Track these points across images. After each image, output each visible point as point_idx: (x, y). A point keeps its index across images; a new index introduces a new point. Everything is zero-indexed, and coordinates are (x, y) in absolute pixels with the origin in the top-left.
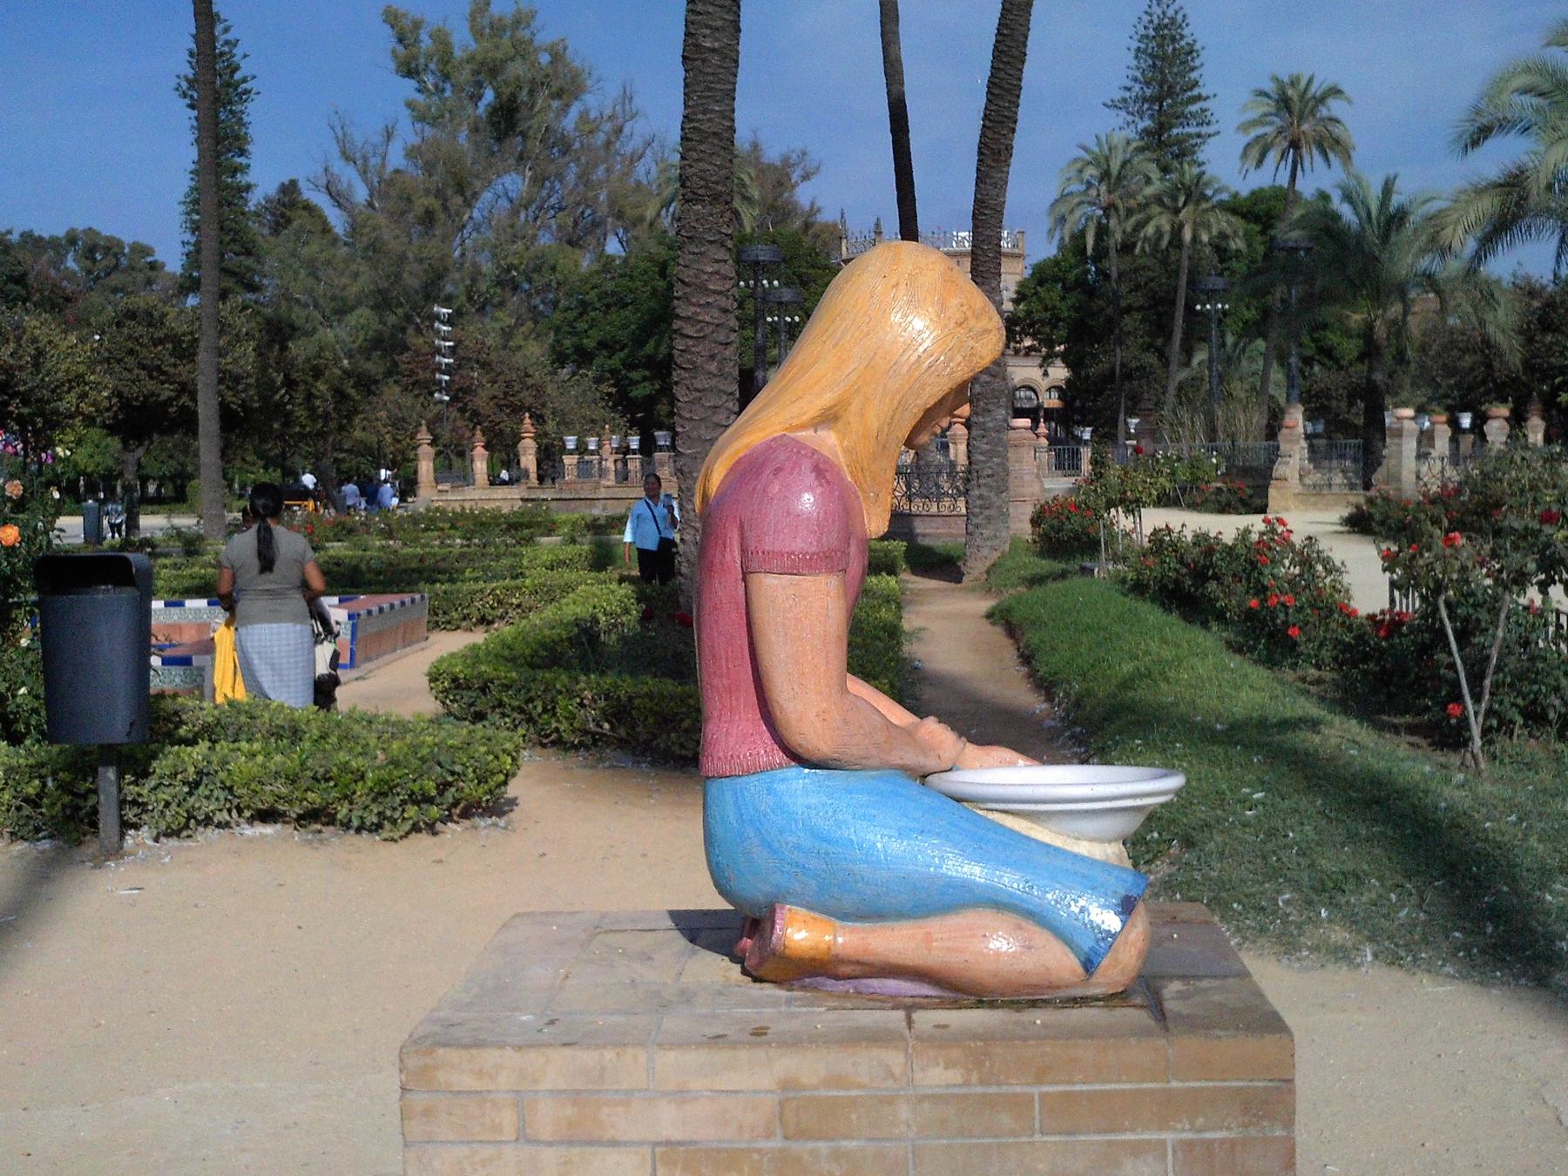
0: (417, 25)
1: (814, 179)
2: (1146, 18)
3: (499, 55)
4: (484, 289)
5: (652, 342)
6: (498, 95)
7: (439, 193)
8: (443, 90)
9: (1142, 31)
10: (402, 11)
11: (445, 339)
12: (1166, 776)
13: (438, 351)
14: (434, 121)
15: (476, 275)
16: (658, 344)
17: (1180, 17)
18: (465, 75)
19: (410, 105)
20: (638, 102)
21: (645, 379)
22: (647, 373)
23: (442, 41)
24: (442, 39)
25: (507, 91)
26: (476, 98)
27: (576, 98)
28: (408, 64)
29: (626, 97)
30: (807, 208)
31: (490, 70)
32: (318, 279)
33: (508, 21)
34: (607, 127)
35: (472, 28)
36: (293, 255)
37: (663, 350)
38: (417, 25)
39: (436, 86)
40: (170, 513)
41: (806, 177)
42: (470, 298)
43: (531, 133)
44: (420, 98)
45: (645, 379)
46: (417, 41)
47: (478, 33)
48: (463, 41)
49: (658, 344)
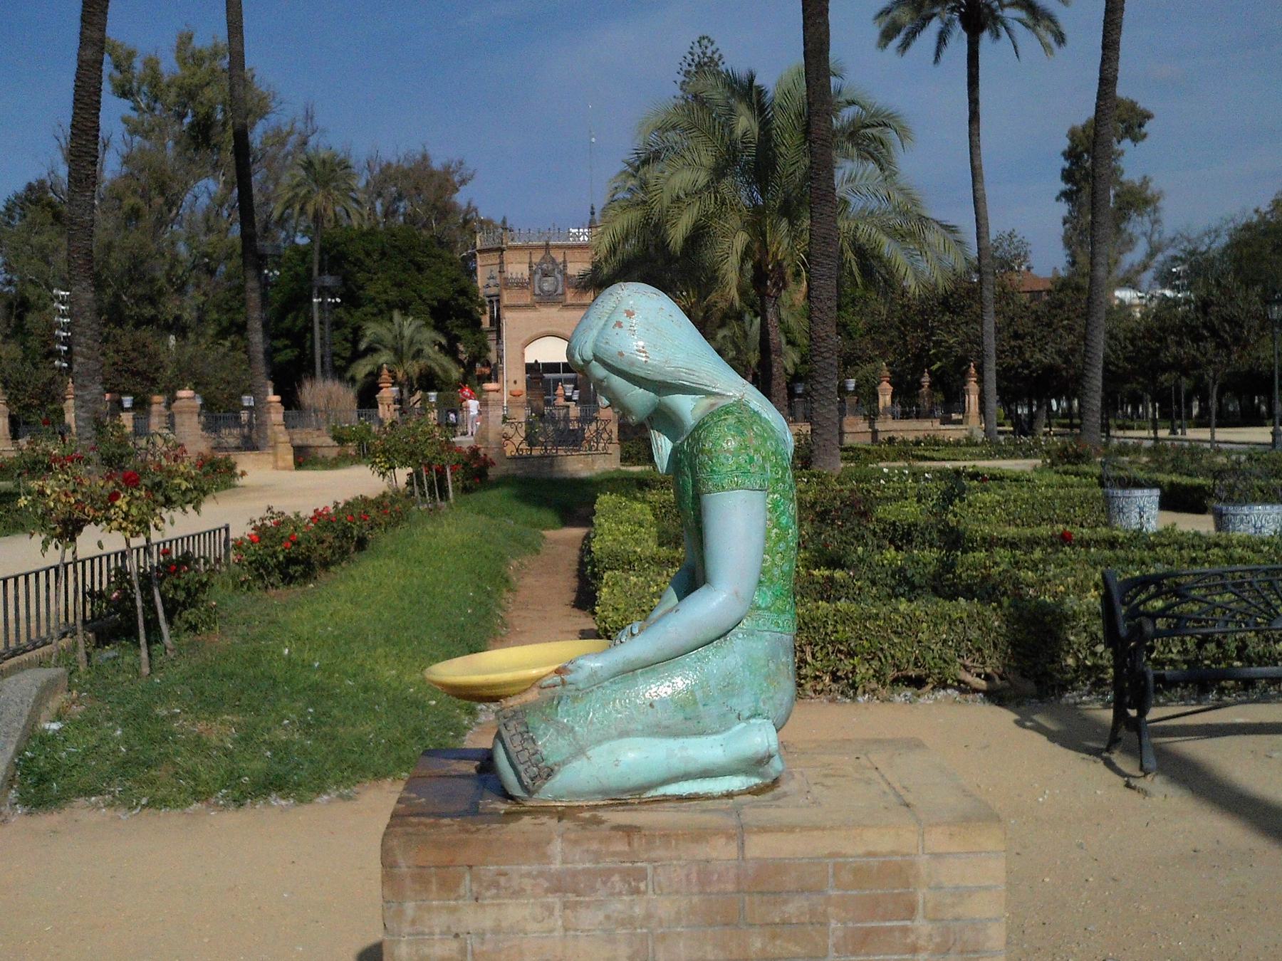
0: (131, 55)
1: (470, 184)
2: (689, 57)
3: (196, 81)
4: (180, 272)
5: (290, 317)
6: (195, 115)
7: (145, 196)
8: (153, 110)
9: (686, 67)
10: (118, 42)
11: (64, 316)
12: (603, 651)
13: (58, 326)
14: (146, 135)
15: (175, 260)
16: (295, 319)
17: (716, 56)
18: (172, 97)
19: (125, 120)
20: (319, 121)
21: (286, 347)
22: (287, 342)
23: (152, 65)
24: (152, 65)
25: (202, 111)
26: (182, 116)
27: (261, 118)
28: (124, 86)
29: (309, 117)
30: (465, 208)
31: (189, 94)
32: (48, 263)
33: (206, 53)
34: (293, 139)
35: (177, 58)
36: (27, 243)
37: (300, 323)
38: (131, 55)
39: (148, 106)
40: (626, 472)
41: (463, 182)
42: (170, 281)
43: (223, 146)
44: (134, 114)
45: (286, 347)
46: (130, 67)
47: (182, 61)
48: (169, 67)
49: (295, 319)
